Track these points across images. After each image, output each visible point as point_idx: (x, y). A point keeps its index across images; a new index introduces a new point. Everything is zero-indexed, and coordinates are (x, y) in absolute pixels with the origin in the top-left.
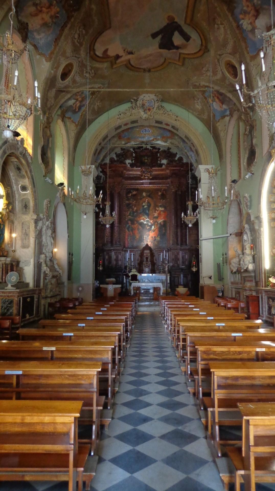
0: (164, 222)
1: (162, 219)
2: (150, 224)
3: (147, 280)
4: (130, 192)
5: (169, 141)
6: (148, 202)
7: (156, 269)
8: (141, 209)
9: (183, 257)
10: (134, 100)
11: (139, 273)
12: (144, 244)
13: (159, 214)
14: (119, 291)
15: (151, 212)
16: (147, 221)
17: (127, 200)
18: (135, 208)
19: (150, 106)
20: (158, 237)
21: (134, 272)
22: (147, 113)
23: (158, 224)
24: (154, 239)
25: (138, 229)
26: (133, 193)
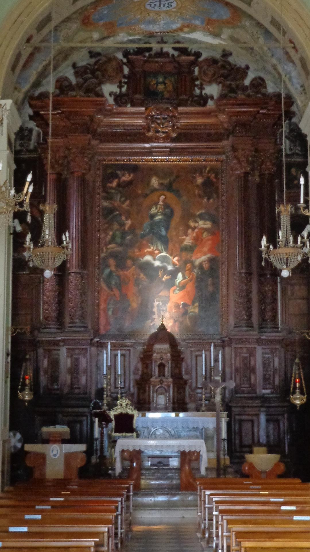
1: (205, 254)
2: (170, 268)
3: (161, 431)
5: (227, 32)
6: (166, 206)
7: (187, 400)
8: (146, 224)
9: (265, 364)
11: (139, 410)
13: (198, 240)
15: (174, 233)
16: (164, 259)
17: (106, 199)
18: (129, 222)
20: (193, 303)
23: (193, 266)
24: (182, 311)
25: (137, 282)
26: (124, 178)
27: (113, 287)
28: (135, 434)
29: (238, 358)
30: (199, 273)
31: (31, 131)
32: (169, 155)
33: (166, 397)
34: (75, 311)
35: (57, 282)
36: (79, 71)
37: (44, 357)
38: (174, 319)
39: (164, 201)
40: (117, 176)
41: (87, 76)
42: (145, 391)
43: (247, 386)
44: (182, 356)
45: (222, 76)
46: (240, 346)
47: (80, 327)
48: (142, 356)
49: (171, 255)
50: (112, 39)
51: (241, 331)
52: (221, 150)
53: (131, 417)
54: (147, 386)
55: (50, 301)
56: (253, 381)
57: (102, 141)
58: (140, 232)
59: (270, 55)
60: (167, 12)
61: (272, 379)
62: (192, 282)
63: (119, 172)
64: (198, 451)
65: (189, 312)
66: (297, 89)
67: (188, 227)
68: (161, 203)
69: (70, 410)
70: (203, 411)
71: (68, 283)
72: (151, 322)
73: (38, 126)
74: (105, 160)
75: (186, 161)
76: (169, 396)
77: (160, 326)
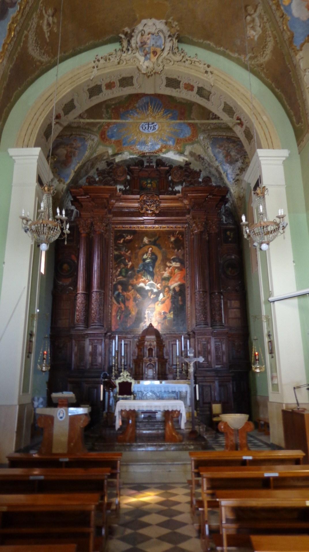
0: (182, 287)
1: (176, 282)
2: (155, 290)
3: (151, 394)
4: (122, 237)
5: (188, 149)
6: (153, 254)
7: (167, 372)
8: (141, 263)
9: (217, 349)
10: (126, 34)
12: (144, 325)
13: (172, 274)
14: (82, 424)
15: (158, 270)
16: (151, 285)
17: (116, 250)
18: (130, 263)
19: (157, 46)
20: (170, 312)
21: (125, 377)
22: (150, 59)
23: (170, 290)
24: (163, 316)
25: (135, 299)
26: (127, 238)
27: (120, 302)
28: (132, 396)
29: (200, 345)
30: (173, 294)
31: (72, 211)
32: (154, 224)
33: (153, 370)
34: (95, 315)
35: (84, 298)
36: (100, 173)
37: (75, 345)
38: (158, 322)
39: (151, 251)
40: (123, 237)
41: (105, 175)
42: (139, 367)
43: (206, 363)
44: (164, 344)
45: (186, 175)
46: (200, 337)
47: (98, 325)
48: (138, 344)
49: (156, 283)
50: (120, 156)
51: (201, 327)
52: (185, 221)
53: (130, 384)
54: (141, 363)
55: (80, 310)
56: (209, 359)
57: (114, 216)
58: (136, 269)
59: (215, 159)
60: (152, 134)
61: (221, 358)
62: (169, 299)
63: (124, 234)
64: (178, 410)
65: (167, 317)
66: (230, 181)
67: (166, 266)
68: (149, 252)
69: (90, 379)
70: (178, 380)
71: (92, 298)
72: (144, 323)
73: (77, 209)
74: (116, 228)
75: (164, 228)
76: (156, 369)
77: (150, 325)
